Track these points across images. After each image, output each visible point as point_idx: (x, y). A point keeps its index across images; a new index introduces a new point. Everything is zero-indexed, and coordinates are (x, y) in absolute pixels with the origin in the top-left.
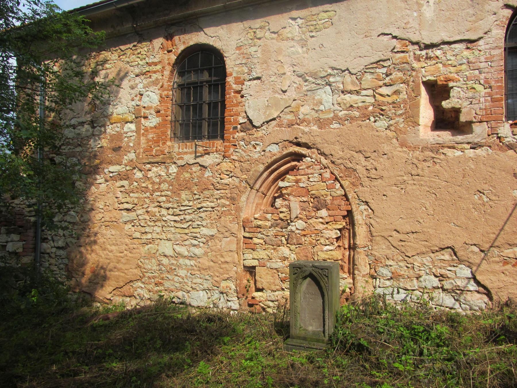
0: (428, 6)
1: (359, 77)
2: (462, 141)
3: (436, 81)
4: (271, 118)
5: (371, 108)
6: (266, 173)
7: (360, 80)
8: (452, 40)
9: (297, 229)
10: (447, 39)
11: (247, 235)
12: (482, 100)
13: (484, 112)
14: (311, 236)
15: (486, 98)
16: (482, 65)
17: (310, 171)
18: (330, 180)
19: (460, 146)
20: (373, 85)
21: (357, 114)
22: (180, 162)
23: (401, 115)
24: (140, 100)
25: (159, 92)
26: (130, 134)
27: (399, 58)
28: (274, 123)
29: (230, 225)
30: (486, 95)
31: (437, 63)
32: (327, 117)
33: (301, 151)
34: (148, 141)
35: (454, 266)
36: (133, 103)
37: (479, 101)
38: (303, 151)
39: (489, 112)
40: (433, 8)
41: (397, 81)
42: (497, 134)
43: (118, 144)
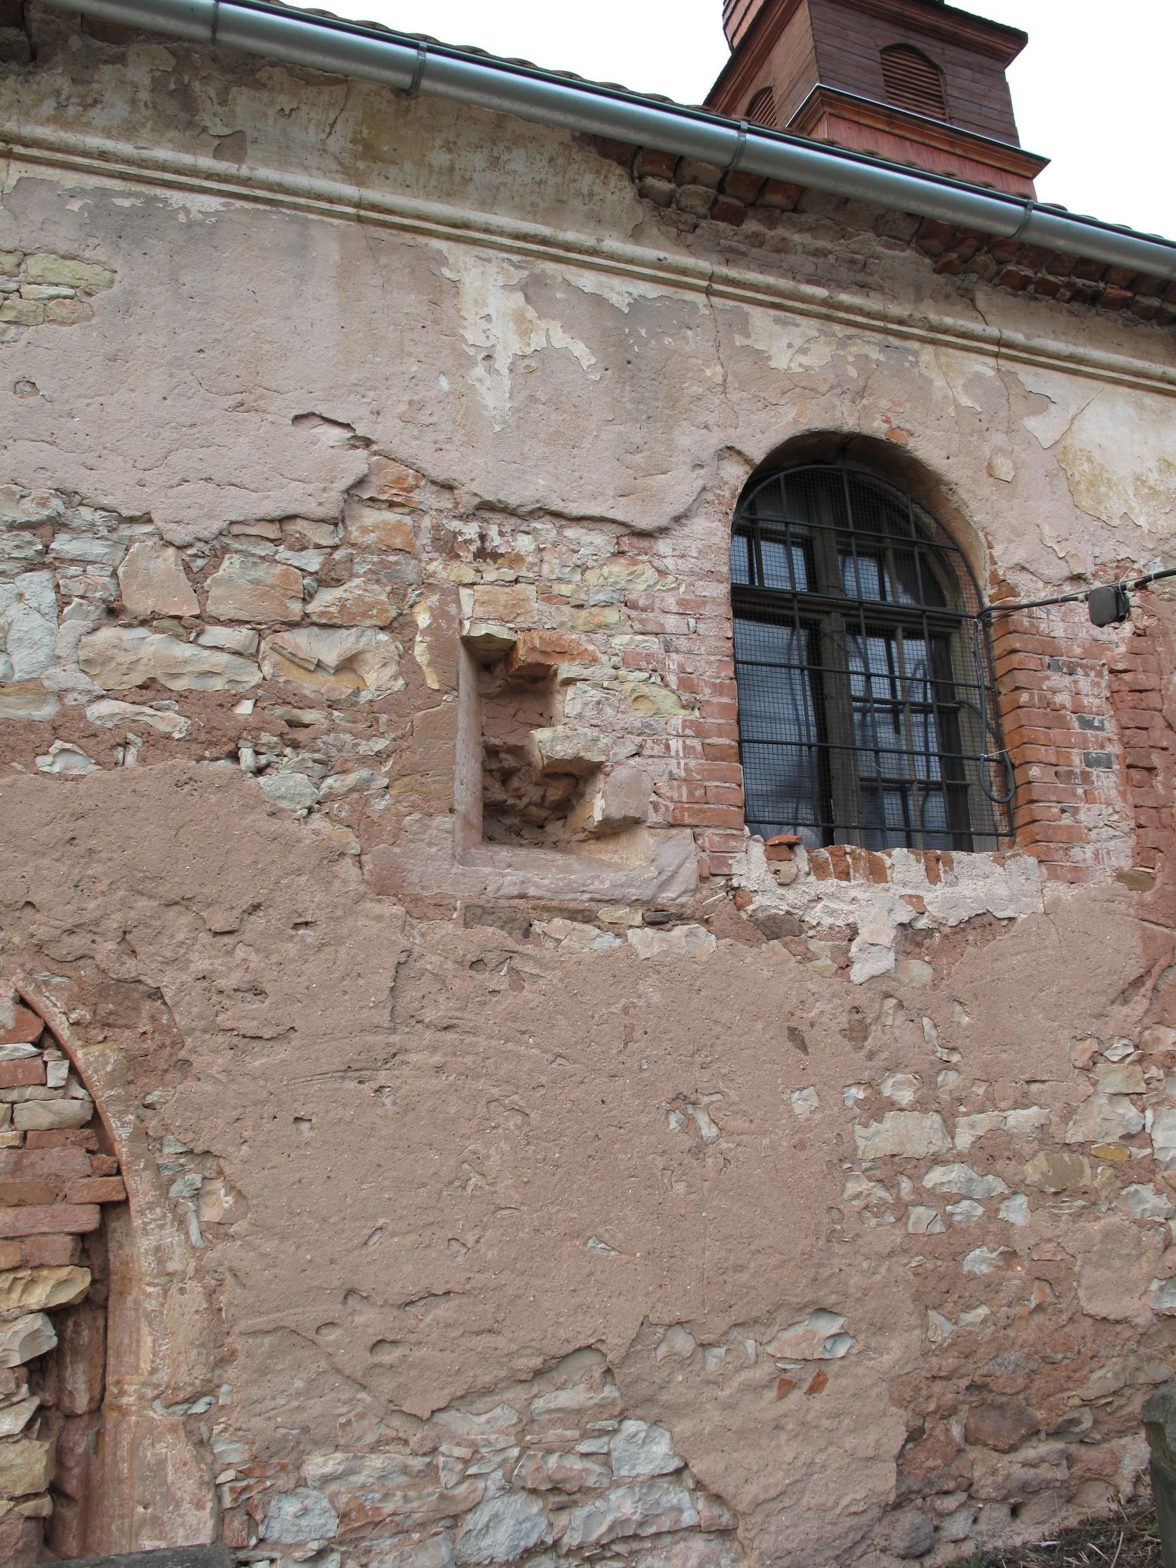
0: (490, 370)
1: (200, 562)
2: (617, 894)
3: (512, 646)
5: (245, 708)
7: (196, 578)
8: (574, 509)
10: (557, 505)
12: (676, 744)
13: (684, 791)
15: (688, 742)
16: (671, 623)
19: (606, 914)
20: (266, 610)
21: (171, 722)
23: (380, 757)
27: (375, 528)
30: (688, 732)
31: (516, 581)
32: (21, 713)
35: (603, 1432)
37: (668, 747)
39: (699, 792)
40: (507, 383)
41: (364, 615)
42: (729, 877)
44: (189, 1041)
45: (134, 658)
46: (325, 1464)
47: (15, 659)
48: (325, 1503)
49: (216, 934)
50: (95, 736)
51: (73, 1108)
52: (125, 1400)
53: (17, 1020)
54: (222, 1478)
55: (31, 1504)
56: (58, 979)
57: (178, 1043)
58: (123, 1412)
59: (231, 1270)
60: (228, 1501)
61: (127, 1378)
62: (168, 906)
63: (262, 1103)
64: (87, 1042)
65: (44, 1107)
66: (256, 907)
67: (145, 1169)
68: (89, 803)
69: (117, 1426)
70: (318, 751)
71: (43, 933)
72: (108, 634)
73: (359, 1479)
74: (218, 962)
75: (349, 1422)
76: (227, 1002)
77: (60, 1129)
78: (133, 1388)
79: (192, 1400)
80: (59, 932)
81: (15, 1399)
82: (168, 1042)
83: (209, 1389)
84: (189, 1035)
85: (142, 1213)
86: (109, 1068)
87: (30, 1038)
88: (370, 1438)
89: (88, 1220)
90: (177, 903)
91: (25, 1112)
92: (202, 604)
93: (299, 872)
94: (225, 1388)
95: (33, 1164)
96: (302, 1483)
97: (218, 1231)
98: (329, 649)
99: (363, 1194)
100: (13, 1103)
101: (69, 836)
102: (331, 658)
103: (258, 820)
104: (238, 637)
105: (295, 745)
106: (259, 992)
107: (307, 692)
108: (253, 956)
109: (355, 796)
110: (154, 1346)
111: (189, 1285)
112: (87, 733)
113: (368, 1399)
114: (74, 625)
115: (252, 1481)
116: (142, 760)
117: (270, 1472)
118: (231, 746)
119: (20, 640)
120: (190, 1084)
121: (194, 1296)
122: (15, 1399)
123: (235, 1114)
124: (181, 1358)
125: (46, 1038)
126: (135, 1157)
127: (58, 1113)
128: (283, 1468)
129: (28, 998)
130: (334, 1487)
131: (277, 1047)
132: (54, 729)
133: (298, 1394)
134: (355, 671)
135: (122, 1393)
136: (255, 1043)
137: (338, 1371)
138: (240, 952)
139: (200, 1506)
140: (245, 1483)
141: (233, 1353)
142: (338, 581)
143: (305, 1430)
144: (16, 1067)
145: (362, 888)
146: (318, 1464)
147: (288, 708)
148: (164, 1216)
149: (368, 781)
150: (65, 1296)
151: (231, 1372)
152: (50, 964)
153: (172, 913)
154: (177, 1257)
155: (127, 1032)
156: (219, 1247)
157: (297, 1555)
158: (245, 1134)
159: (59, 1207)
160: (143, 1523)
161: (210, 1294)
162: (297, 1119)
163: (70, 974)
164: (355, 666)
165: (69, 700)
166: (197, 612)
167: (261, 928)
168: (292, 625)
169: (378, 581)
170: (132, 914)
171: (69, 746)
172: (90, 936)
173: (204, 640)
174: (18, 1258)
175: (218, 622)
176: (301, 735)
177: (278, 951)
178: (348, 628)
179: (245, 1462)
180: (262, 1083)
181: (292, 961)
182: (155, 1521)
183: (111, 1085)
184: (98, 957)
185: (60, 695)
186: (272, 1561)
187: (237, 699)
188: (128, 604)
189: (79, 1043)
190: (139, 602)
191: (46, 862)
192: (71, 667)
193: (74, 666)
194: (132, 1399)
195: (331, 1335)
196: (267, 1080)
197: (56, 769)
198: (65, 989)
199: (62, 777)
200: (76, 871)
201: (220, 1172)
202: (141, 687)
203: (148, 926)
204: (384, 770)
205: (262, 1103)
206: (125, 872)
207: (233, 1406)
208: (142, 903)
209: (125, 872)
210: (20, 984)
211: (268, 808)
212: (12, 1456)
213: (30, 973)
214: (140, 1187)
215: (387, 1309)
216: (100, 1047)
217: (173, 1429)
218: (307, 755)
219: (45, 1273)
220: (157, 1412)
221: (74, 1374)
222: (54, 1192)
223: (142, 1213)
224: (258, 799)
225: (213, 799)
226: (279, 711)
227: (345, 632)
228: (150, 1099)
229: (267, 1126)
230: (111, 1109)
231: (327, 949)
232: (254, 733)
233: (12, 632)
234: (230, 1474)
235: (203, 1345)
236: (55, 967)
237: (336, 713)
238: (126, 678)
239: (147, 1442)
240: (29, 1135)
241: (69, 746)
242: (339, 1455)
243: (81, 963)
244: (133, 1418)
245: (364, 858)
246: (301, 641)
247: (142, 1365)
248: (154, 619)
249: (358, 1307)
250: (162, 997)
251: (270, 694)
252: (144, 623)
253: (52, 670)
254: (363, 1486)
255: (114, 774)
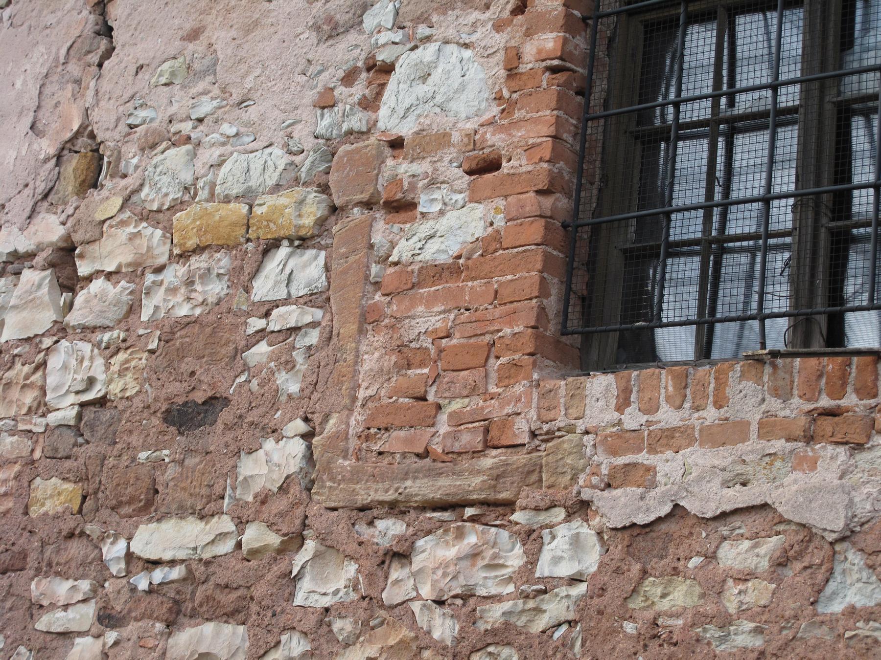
22: (620, 506)
24: (370, 104)
25: (499, 40)
26: (287, 316)
29: (234, 96)
34: (406, 356)
36: (326, 122)
43: (209, 380)
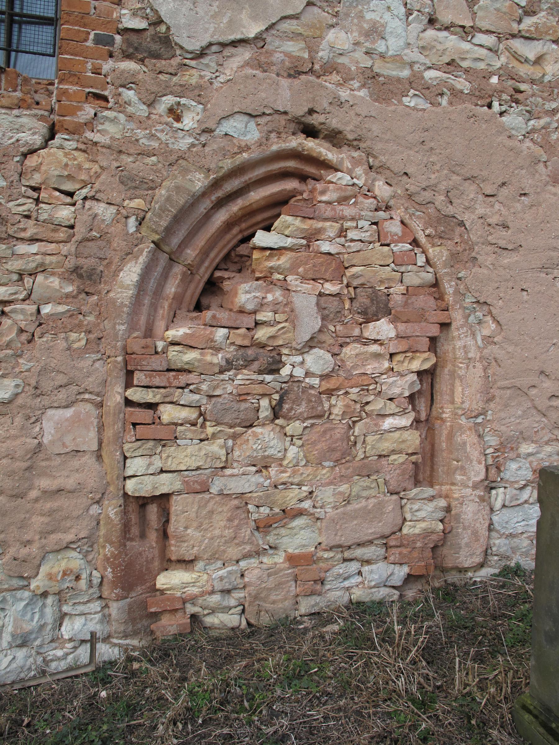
4: (239, 36)
5: (494, 80)
6: (206, 204)
9: (308, 374)
11: (135, 395)
14: (347, 393)
17: (348, 211)
18: (401, 240)
20: (502, 26)
21: (462, 84)
28: (245, 54)
32: (394, 73)
33: (323, 151)
38: (311, 170)
41: (547, 33)
44: (476, 248)
45: (445, 48)
46: (528, 448)
47: (389, 43)
48: (528, 465)
49: (487, 196)
50: (428, 88)
51: (429, 277)
52: (444, 416)
53: (402, 232)
54: (488, 451)
55: (415, 457)
56: (419, 213)
57: (472, 249)
58: (443, 420)
59: (494, 358)
60: (490, 461)
61: (446, 406)
62: (465, 180)
63: (507, 280)
64: (433, 246)
65: (417, 275)
66: (504, 184)
67: (459, 308)
68: (430, 124)
69: (441, 426)
70: (527, 106)
71: (413, 189)
72: (431, 33)
73: (541, 456)
74: (488, 210)
75: (538, 431)
76: (492, 230)
77: (422, 287)
78: (448, 410)
79: (476, 417)
80: (420, 189)
81: (407, 411)
82: (467, 248)
83: (483, 413)
84: (477, 245)
85: (458, 329)
86: (444, 259)
87: (409, 241)
88: (546, 439)
89: (434, 331)
90: (469, 179)
91: (408, 277)
92: (473, 20)
93: (522, 168)
94: (490, 412)
95: (413, 303)
96: (519, 456)
97: (489, 340)
98: (530, 51)
99: (548, 327)
100: (402, 273)
101: (422, 140)
102: (532, 56)
103: (502, 138)
104: (489, 40)
105: (517, 102)
106: (506, 227)
107: (522, 74)
108: (502, 208)
109: (544, 131)
110: (461, 392)
111: (477, 364)
112: (426, 87)
113: (546, 421)
114: (416, 27)
115: (500, 454)
116: (451, 103)
117: (507, 451)
118: (488, 100)
119: (391, 32)
120: (476, 269)
121: (478, 371)
122: (407, 411)
123: (497, 285)
124: (474, 397)
125: (415, 243)
126: (456, 302)
127: (422, 279)
128: (512, 449)
129: (405, 221)
130: (531, 458)
131: (514, 254)
132: (410, 83)
133: (519, 417)
134: (540, 65)
135: (443, 412)
136: (504, 252)
137: (536, 408)
138: (497, 206)
139: (480, 463)
140: (497, 454)
141: (494, 397)
142: (534, 12)
143: (521, 433)
144: (404, 255)
145: (548, 179)
146: (526, 448)
147: (514, 81)
148: (467, 331)
149: (549, 124)
150: (427, 366)
151: (492, 405)
152: (415, 205)
153: (467, 184)
154: (472, 351)
155: (449, 242)
156: (489, 347)
157: (516, 486)
158: (501, 295)
159: (423, 324)
160: (457, 468)
161: (485, 370)
162: (522, 290)
163: (424, 211)
164: (540, 62)
165: (416, 67)
166: (472, 25)
167: (506, 194)
168: (513, 36)
169: (552, 15)
170: (451, 183)
171: (417, 93)
172: (433, 192)
173: (475, 41)
174: (407, 347)
175: (481, 31)
176: (519, 96)
177: (513, 207)
178: (538, 40)
179: (497, 445)
180: (508, 271)
181: (519, 212)
182: (462, 468)
183: (445, 267)
184: (436, 203)
185: (411, 65)
186: (505, 488)
187: (492, 74)
188: (439, 18)
189: (430, 245)
190: (446, 17)
191: (412, 153)
192: (415, 50)
193: (417, 49)
194: (447, 415)
195: (534, 392)
196: (510, 270)
197: (412, 104)
198: (422, 218)
199: (414, 109)
200: (425, 158)
201: (490, 313)
202: (448, 64)
203: (458, 189)
204: (555, 119)
205: (507, 280)
206: (447, 161)
207: (493, 421)
208: (454, 177)
209: (447, 161)
210: (402, 214)
211: (508, 134)
212: (406, 436)
213: (406, 209)
214: (457, 317)
215: (555, 382)
216: (439, 248)
217: (470, 429)
218: (523, 108)
219: (418, 354)
220: (463, 421)
221: (419, 403)
222: (421, 317)
223: (458, 329)
224: (502, 129)
225: (484, 126)
226: (510, 82)
227: (536, 42)
228: (460, 275)
229: (510, 292)
230: (445, 278)
231: (534, 208)
232: (499, 94)
233: (387, 28)
234: (490, 450)
235: (482, 392)
236: (417, 207)
237: (534, 86)
238: (441, 58)
239: (459, 434)
240: (410, 289)
241: (417, 93)
242: (534, 445)
243: (428, 205)
244: (448, 424)
245: (548, 163)
246: (517, 44)
247: (456, 399)
248: (452, 27)
249: (544, 380)
250: (464, 225)
251: (508, 74)
252: (447, 29)
253: (406, 51)
254: (542, 459)
255: (439, 110)
